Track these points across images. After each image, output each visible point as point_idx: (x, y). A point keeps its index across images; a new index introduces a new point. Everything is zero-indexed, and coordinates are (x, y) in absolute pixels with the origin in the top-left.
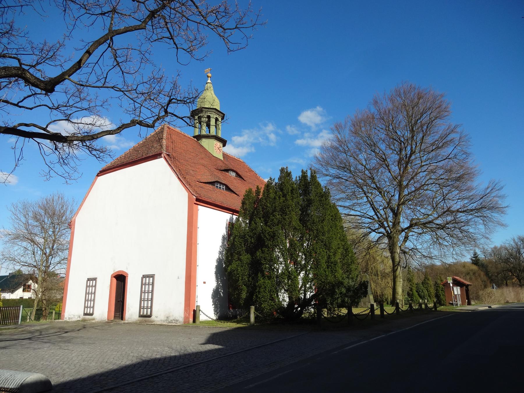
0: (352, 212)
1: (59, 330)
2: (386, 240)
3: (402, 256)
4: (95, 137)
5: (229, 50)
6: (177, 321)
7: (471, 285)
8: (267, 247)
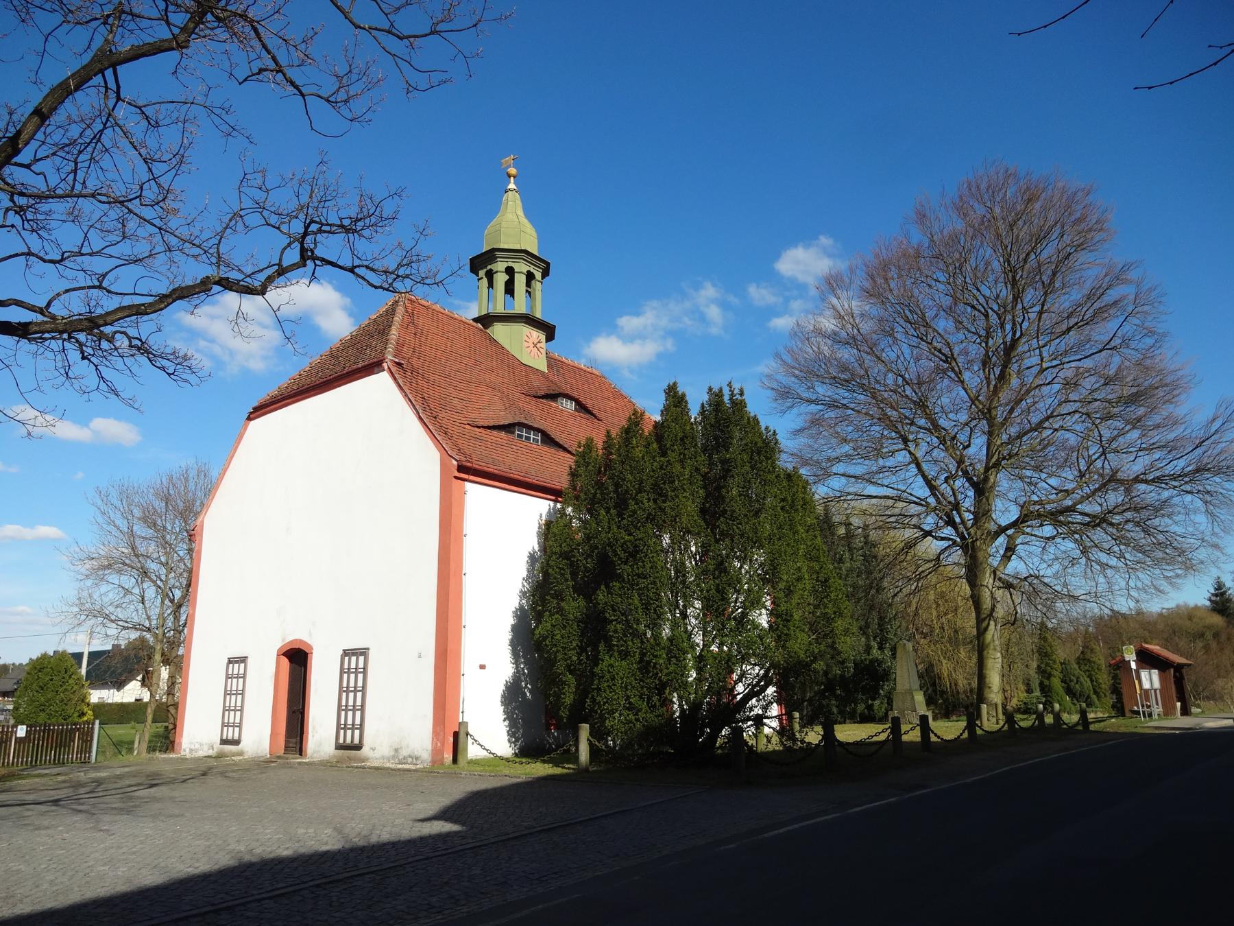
0: (871, 490)
2: (957, 556)
3: (999, 594)
5: (410, 88)
7: (1189, 665)
8: (619, 577)
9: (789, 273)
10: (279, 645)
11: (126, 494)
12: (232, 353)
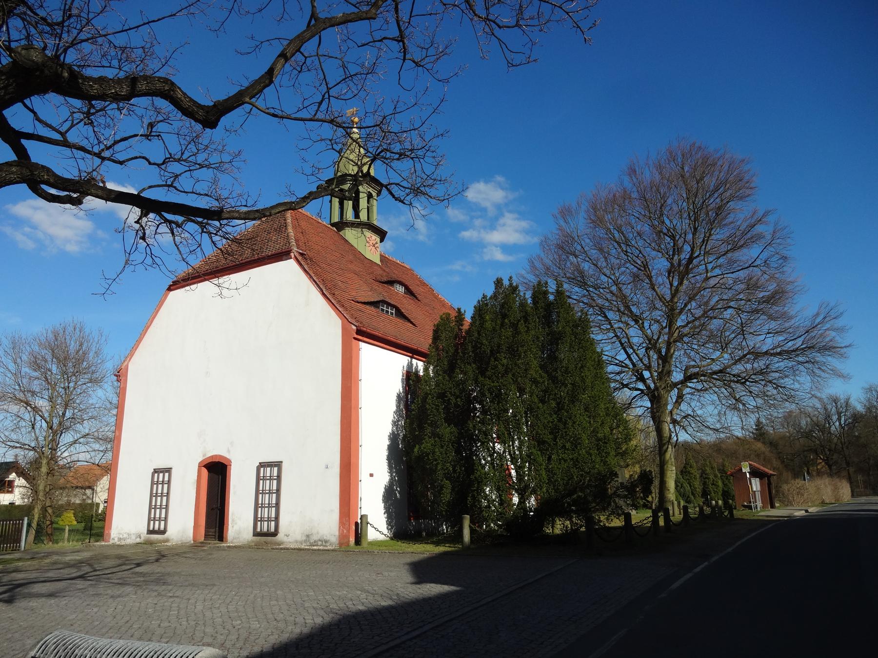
1: (119, 562)
4: (268, 214)
6: (326, 542)
9: (474, 200)
10: (201, 459)
11: (16, 345)
12: (52, 238)
